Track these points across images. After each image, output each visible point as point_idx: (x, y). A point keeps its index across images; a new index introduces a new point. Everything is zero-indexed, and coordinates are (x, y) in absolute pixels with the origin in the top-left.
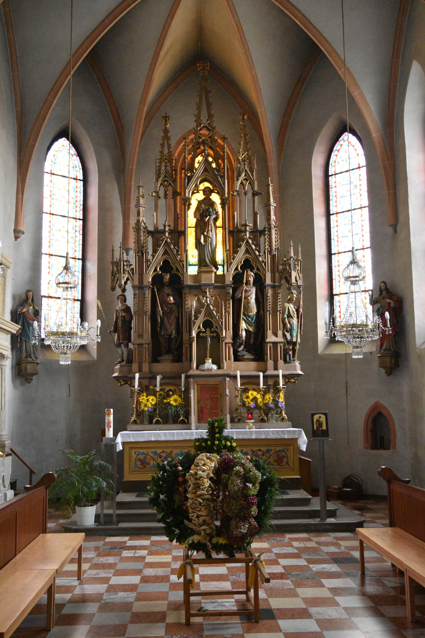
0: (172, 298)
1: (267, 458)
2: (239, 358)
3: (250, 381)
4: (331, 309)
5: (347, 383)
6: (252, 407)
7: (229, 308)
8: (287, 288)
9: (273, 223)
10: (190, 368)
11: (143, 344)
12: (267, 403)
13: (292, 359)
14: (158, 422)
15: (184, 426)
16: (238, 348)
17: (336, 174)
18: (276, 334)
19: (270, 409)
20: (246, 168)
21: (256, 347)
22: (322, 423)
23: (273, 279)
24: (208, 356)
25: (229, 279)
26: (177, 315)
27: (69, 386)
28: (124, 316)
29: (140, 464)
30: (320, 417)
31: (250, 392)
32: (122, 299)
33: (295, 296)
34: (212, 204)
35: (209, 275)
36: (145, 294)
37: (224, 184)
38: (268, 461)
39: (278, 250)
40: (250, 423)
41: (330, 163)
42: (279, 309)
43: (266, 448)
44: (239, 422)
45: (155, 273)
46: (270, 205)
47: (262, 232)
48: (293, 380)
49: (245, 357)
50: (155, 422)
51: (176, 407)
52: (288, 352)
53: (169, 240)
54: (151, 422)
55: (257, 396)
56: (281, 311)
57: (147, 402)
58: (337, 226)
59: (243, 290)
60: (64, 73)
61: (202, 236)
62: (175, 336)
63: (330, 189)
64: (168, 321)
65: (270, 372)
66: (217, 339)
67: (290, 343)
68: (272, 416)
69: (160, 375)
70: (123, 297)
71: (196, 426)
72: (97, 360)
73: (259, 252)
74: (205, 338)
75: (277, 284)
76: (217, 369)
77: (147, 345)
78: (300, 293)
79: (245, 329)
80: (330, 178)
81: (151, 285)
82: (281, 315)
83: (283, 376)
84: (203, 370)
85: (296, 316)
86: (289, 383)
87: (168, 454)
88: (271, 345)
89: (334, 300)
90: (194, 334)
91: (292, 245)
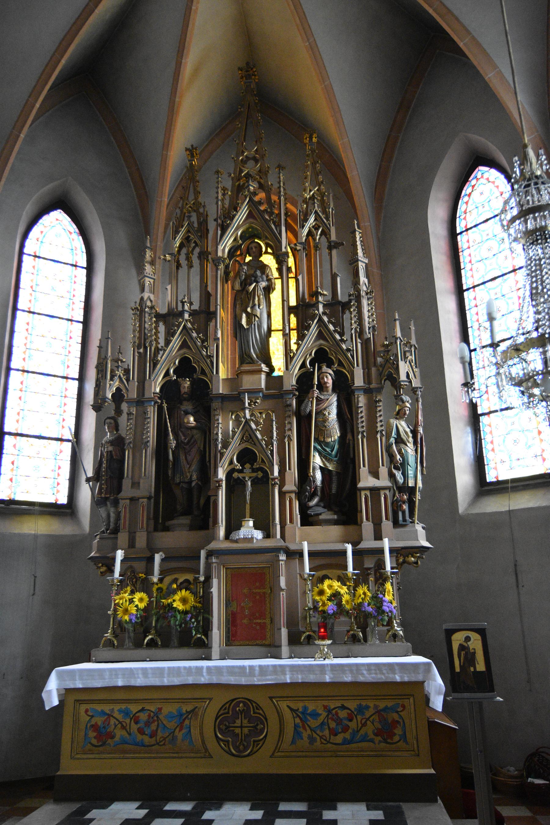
0: (192, 419)
1: (360, 725)
2: (311, 519)
3: (328, 562)
4: (476, 439)
5: (516, 565)
6: (331, 612)
7: (290, 429)
8: (395, 396)
9: (364, 288)
10: (213, 537)
11: (139, 498)
12: (360, 603)
13: (407, 518)
14: (152, 644)
15: (200, 651)
16: (308, 501)
17: (467, 230)
18: (375, 474)
19: (367, 616)
20: (316, 208)
21: (341, 500)
22: (474, 653)
23: (367, 377)
24: (248, 514)
25: (291, 382)
26: (202, 448)
27: (35, 577)
28: (111, 452)
29: (95, 737)
30: (468, 639)
31: (327, 582)
32: (111, 423)
33: (408, 405)
34: (264, 267)
35: (256, 377)
36: (145, 413)
37: (280, 234)
38: (362, 732)
39: (374, 330)
40: (324, 645)
41: (458, 216)
42: (379, 429)
43: (357, 702)
44: (308, 643)
45: (167, 379)
46: (358, 260)
47: (346, 306)
48: (413, 559)
49: (321, 517)
50: (147, 643)
51: (185, 613)
52: (401, 506)
53: (189, 325)
54: (138, 645)
55: (339, 590)
56: (384, 433)
57: (130, 603)
58: (476, 306)
59: (313, 399)
60: (35, 93)
61: (244, 315)
62: (197, 484)
63: (460, 254)
64: (186, 459)
65: (368, 543)
66: (263, 481)
67: (404, 488)
68: (373, 631)
69: (161, 553)
70: (112, 421)
71: (221, 652)
72: (89, 534)
73: (342, 334)
74: (242, 483)
75: (373, 386)
76: (264, 538)
77: (145, 500)
78: (417, 401)
79: (321, 467)
80: (459, 237)
81: (159, 398)
82: (384, 438)
83: (391, 550)
84: (236, 541)
85: (411, 440)
86: (406, 564)
87: (152, 714)
88: (368, 493)
89: (481, 424)
90: (221, 474)
91: (397, 317)
